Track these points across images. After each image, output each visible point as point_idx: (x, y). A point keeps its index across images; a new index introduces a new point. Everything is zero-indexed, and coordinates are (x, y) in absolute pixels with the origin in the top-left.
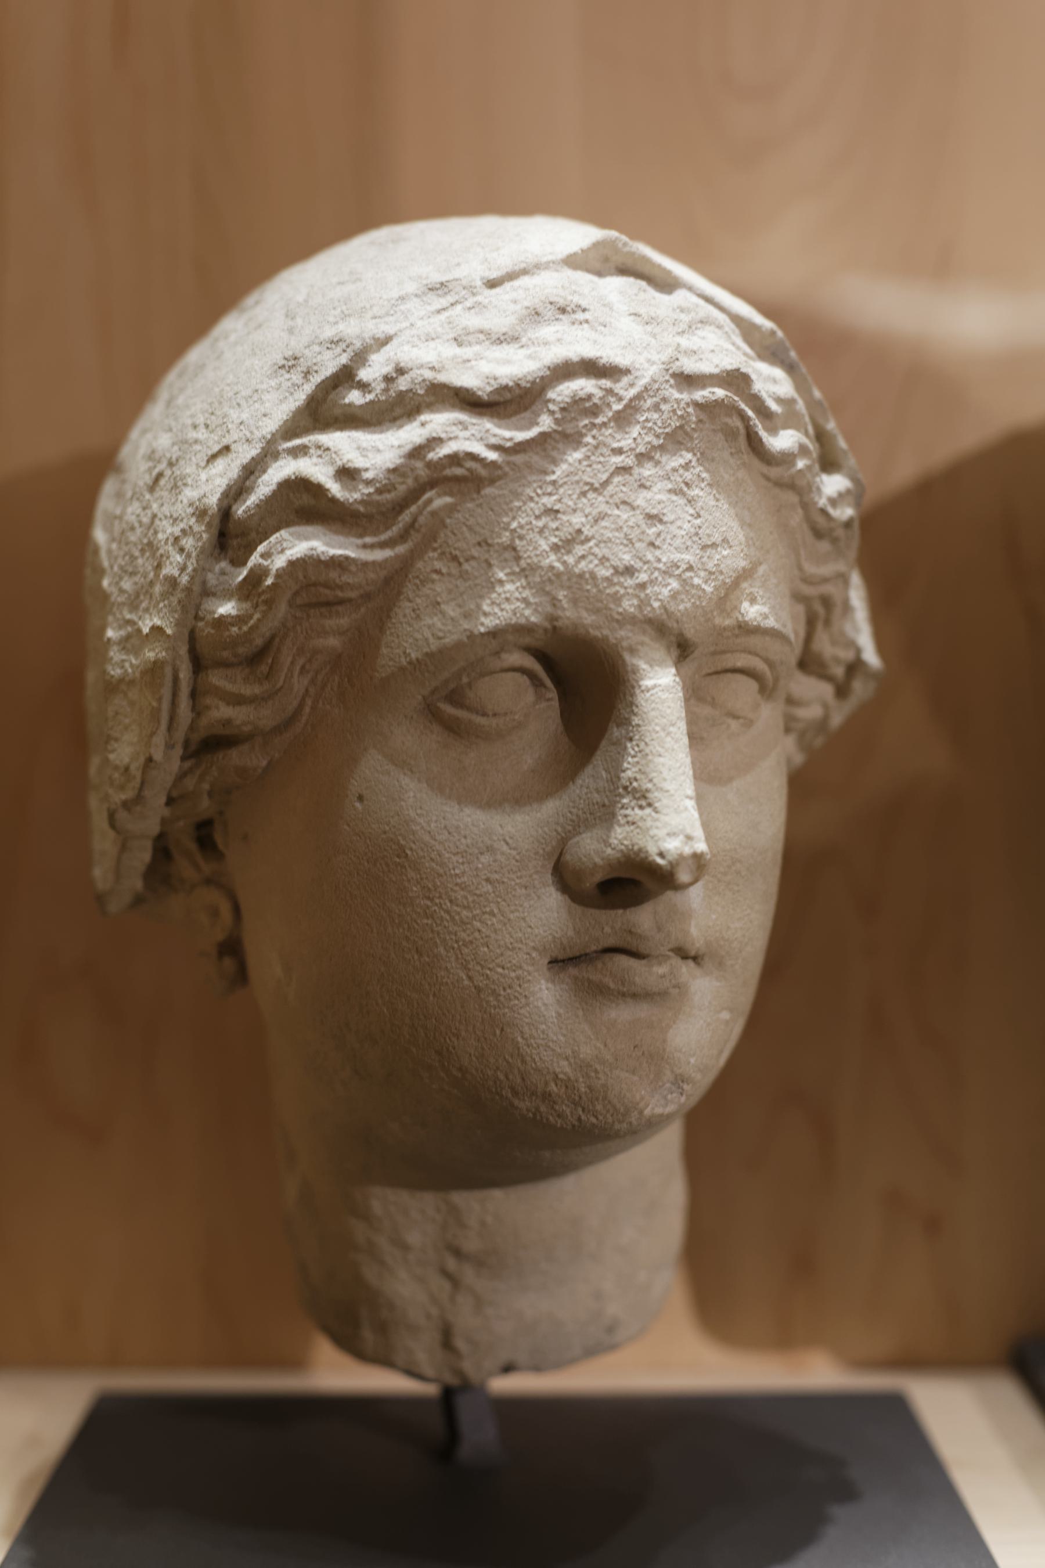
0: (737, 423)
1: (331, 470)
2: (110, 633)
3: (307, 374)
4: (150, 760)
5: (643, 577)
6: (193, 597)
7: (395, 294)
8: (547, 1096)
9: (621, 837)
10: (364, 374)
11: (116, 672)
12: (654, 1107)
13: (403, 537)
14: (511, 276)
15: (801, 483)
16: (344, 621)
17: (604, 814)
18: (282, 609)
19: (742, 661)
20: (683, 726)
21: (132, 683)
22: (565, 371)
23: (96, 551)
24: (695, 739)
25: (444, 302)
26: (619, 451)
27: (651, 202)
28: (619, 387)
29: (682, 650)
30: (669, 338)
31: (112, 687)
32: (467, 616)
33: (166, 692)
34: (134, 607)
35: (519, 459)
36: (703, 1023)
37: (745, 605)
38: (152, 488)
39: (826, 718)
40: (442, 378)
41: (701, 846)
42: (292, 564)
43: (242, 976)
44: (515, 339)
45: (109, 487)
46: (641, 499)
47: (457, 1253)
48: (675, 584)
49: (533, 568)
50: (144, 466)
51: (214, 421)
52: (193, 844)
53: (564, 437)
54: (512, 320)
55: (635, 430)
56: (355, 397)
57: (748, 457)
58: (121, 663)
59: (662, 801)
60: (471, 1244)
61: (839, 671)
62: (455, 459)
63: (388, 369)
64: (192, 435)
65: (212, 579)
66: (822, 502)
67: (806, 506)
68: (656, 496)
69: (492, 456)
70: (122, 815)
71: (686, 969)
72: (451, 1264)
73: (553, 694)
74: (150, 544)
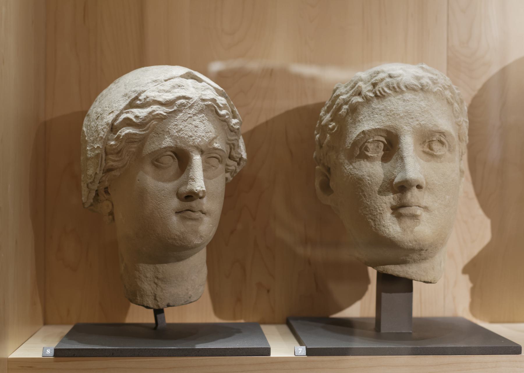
0: (214, 109)
1: (133, 116)
2: (88, 148)
3: (129, 97)
4: (96, 173)
5: (194, 138)
6: (106, 140)
7: (146, 82)
8: (175, 239)
9: (189, 187)
10: (140, 98)
11: (89, 156)
12: (197, 242)
13: (147, 130)
14: (169, 79)
15: (227, 120)
16: (136, 145)
17: (186, 183)
18: (123, 143)
19: (215, 155)
20: (201, 166)
21: (92, 158)
22: (179, 98)
23: (84, 132)
24: (204, 171)
25: (156, 84)
26: (190, 114)
27: (197, 65)
28: (189, 101)
29: (202, 152)
30: (200, 92)
31: (88, 159)
32: (160, 144)
33: (100, 159)
34: (93, 143)
35: (170, 115)
36: (207, 227)
37: (215, 144)
38: (97, 119)
39: (236, 169)
40: (155, 99)
41: (204, 189)
42: (126, 134)
43: (113, 219)
44: (170, 92)
45: (86, 119)
46: (194, 123)
47: (157, 278)
48: (200, 139)
49: (172, 136)
50: (95, 115)
51: (110, 106)
52: (102, 193)
53: (178, 111)
54: (169, 88)
55: (193, 110)
56: (138, 102)
57: (215, 115)
58: (90, 154)
59: (197, 180)
60: (160, 276)
61: (238, 160)
62: (157, 114)
63: (145, 97)
64: (105, 109)
65: (110, 137)
66: (232, 124)
67: (228, 125)
68: (197, 122)
69: (165, 114)
70: (90, 185)
71: (202, 215)
72: (156, 281)
73: (177, 160)
74: (97, 130)
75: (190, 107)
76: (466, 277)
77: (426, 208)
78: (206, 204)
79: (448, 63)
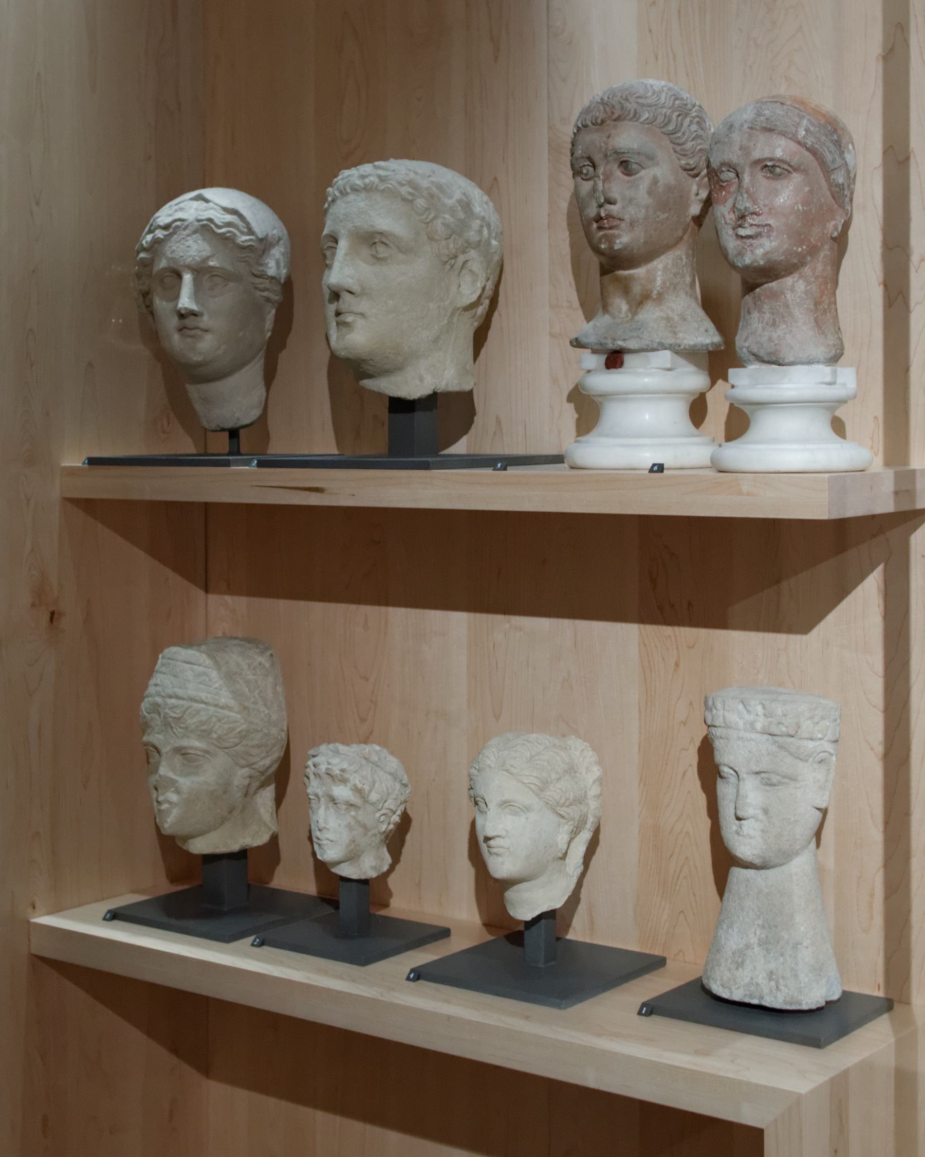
75: (185, 229)
76: (570, 407)
77: (362, 315)
78: (205, 321)
79: (549, 146)
